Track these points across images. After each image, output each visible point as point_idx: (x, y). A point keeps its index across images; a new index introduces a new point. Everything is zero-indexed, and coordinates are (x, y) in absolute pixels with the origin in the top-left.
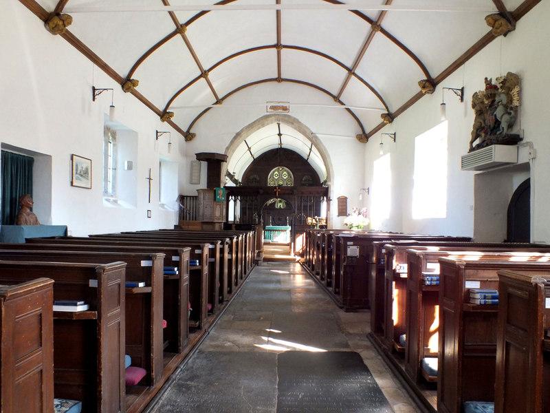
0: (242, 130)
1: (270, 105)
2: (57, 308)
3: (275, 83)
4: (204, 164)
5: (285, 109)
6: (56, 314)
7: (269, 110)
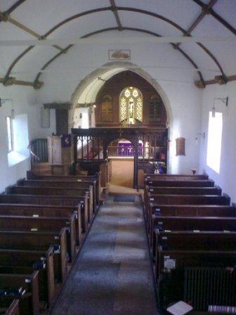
0: (86, 78)
1: (112, 53)
2: (234, 218)
3: (117, 31)
4: (53, 112)
5: (126, 56)
6: (234, 216)
7: (111, 58)
